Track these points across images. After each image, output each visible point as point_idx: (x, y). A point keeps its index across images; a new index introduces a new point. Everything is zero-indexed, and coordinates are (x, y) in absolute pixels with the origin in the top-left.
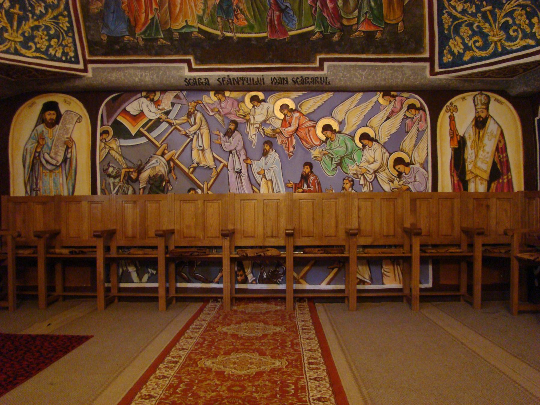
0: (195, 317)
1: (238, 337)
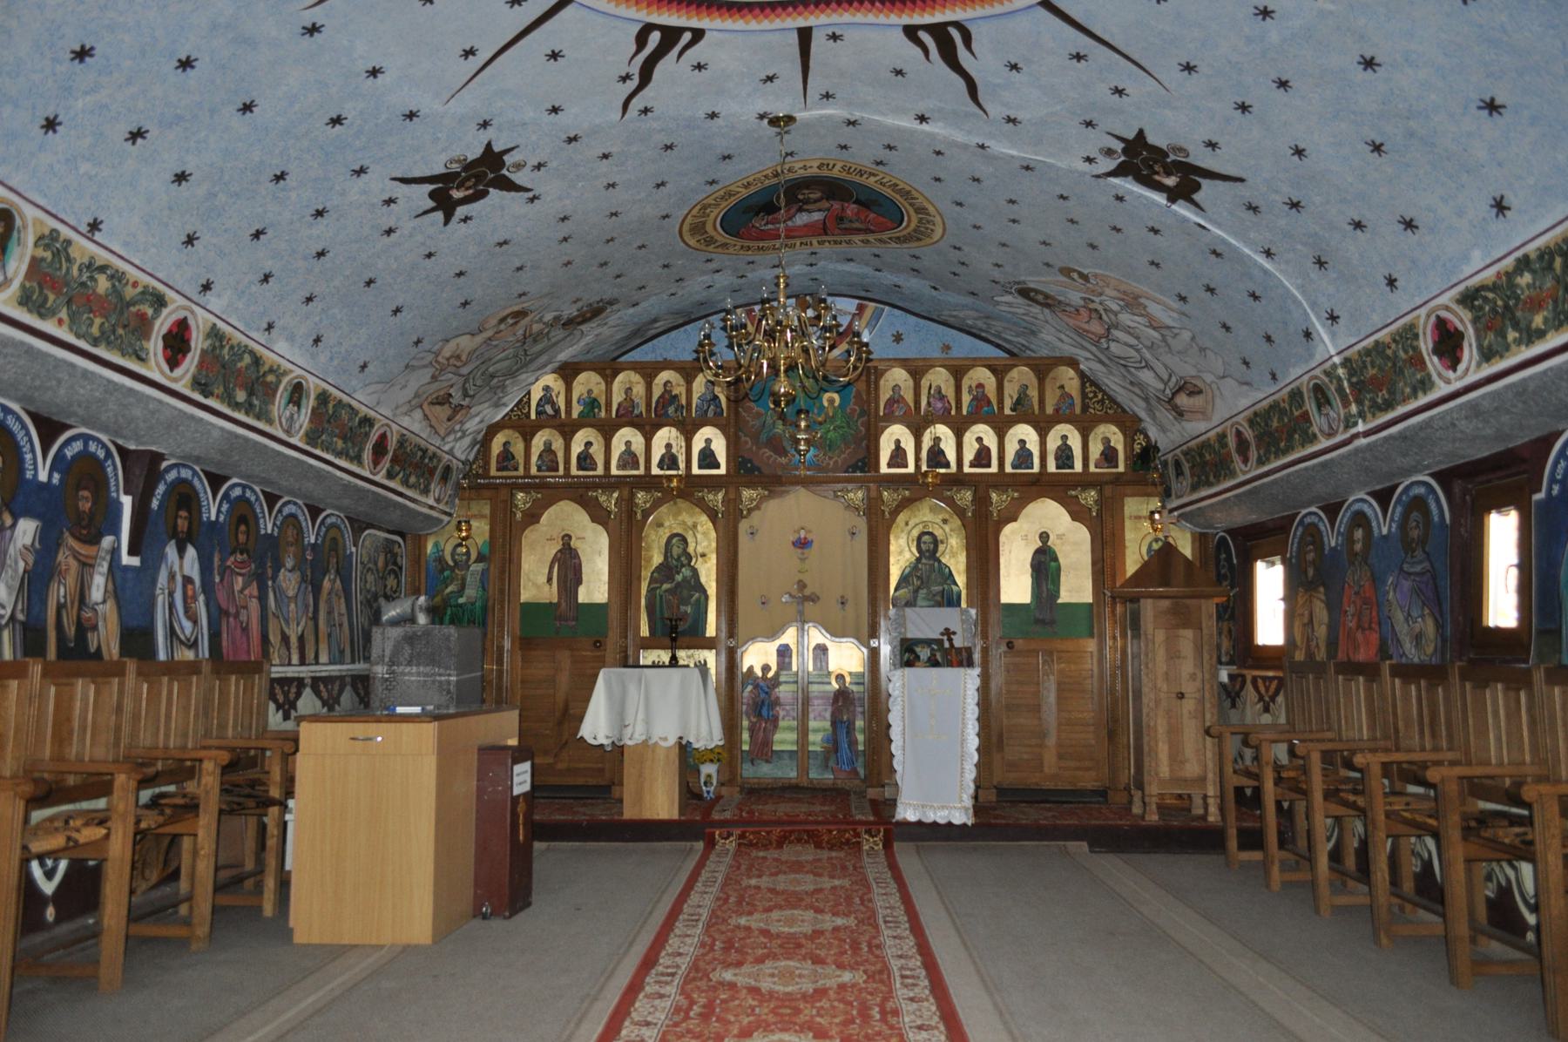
0: (701, 865)
1: (762, 995)
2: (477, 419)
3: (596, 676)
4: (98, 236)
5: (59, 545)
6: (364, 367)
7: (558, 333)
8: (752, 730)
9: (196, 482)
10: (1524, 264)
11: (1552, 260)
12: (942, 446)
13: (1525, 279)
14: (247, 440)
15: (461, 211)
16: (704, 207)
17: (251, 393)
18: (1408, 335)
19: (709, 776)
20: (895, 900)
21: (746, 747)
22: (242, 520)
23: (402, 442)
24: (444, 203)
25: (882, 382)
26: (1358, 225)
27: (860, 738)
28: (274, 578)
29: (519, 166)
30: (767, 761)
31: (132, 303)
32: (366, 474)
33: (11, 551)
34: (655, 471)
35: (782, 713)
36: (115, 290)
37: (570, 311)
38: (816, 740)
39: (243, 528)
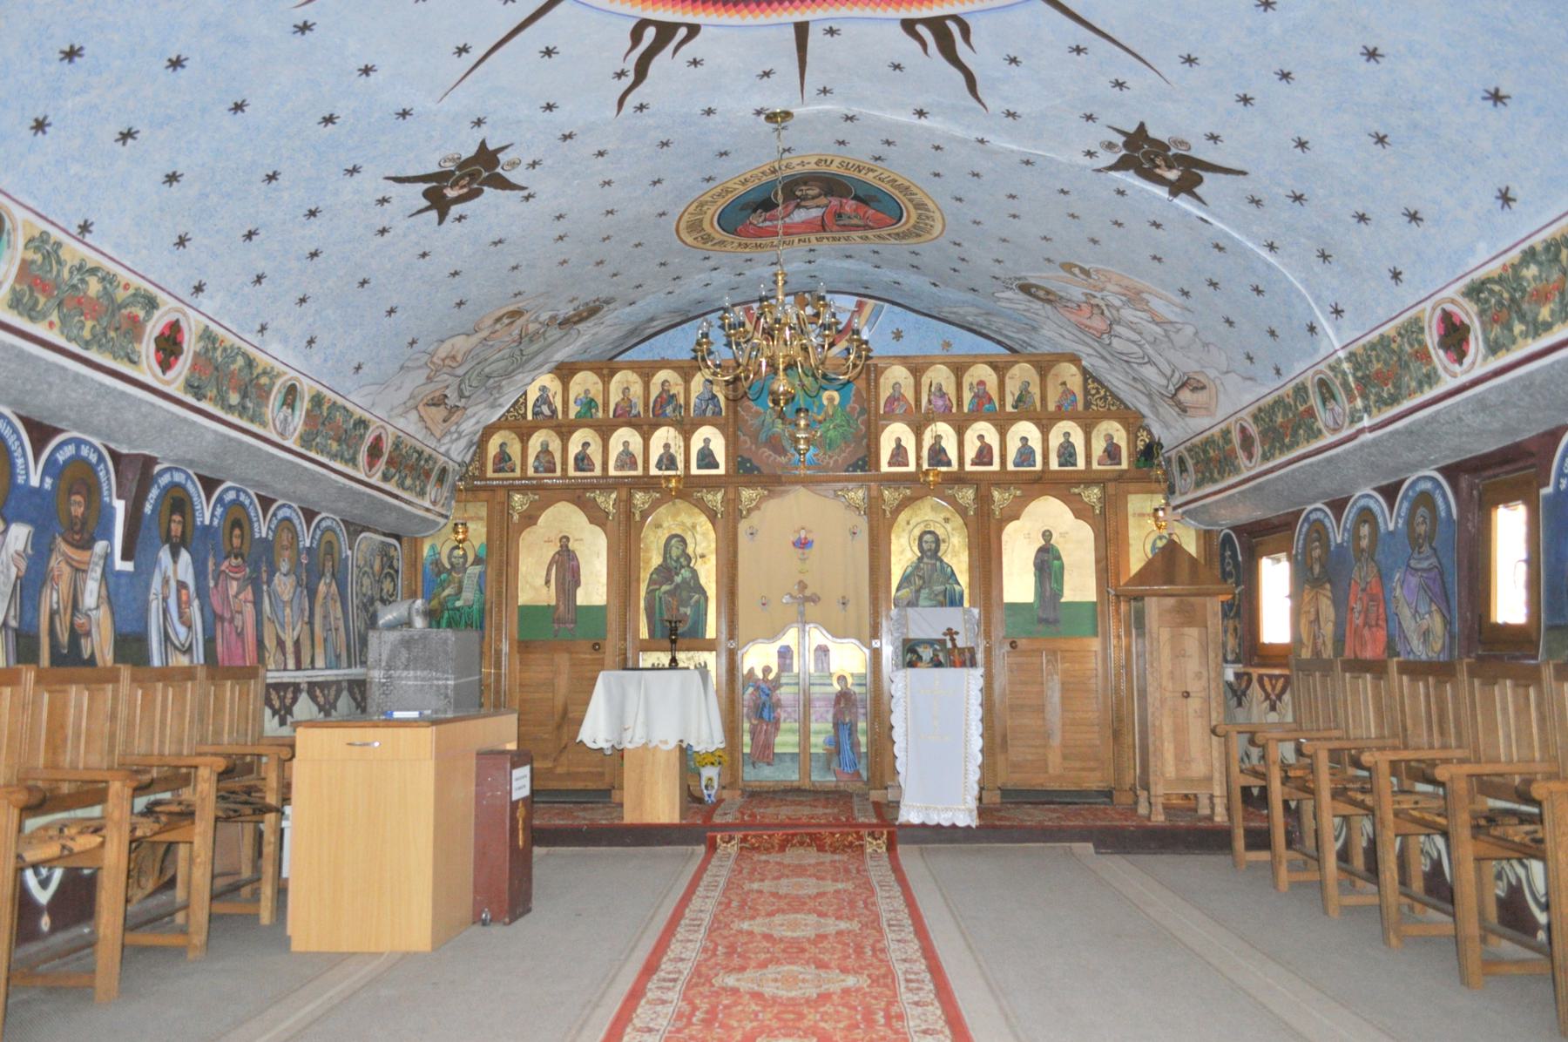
0: (702, 869)
2: (473, 420)
3: (595, 679)
4: (88, 238)
5: (51, 550)
6: (358, 368)
7: (555, 333)
8: (753, 733)
9: (190, 486)
10: (1530, 255)
12: (943, 444)
13: (1532, 271)
14: (240, 443)
15: (455, 210)
16: (701, 205)
17: (244, 396)
18: (1414, 328)
20: (899, 903)
21: (747, 750)
22: (237, 524)
25: (882, 380)
27: (863, 739)
28: (269, 583)
29: (514, 164)
30: (769, 764)
34: (654, 471)
35: (783, 715)
37: (567, 310)
38: (818, 743)
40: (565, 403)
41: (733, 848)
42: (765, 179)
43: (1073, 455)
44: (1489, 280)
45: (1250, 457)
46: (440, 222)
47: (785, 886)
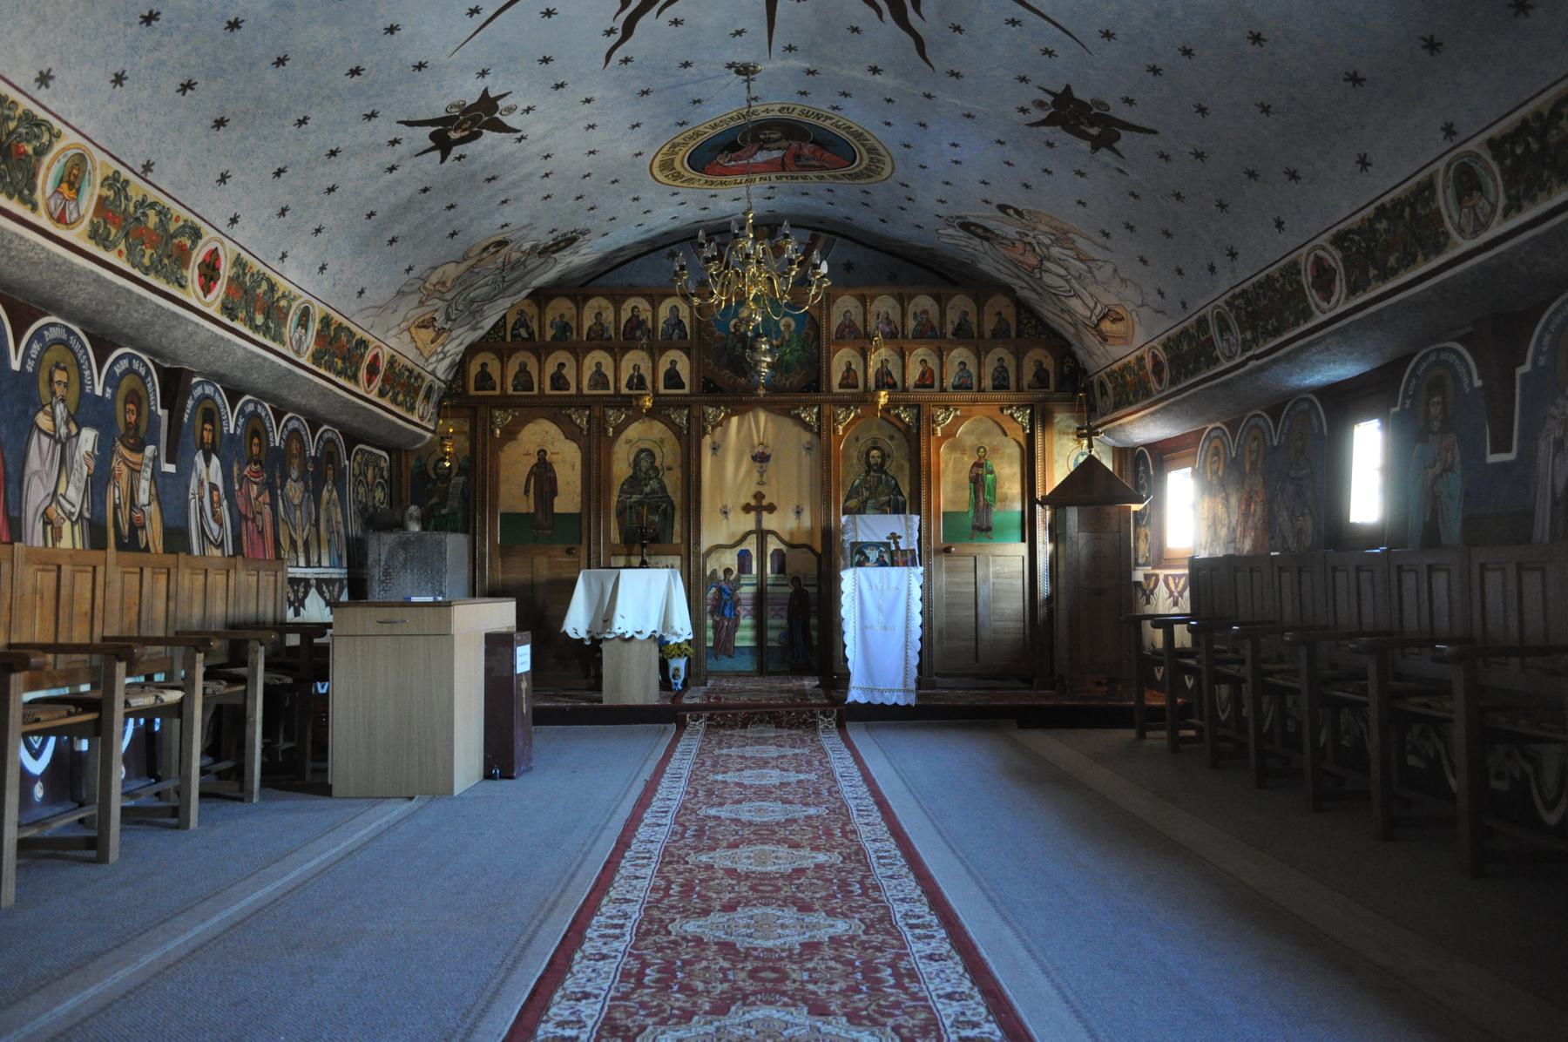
2: (457, 342)
3: (573, 583)
4: (150, 177)
5: (113, 453)
6: (361, 292)
7: (534, 262)
8: (716, 627)
9: (217, 398)
10: (1381, 212)
11: (1403, 211)
13: (1382, 225)
14: (265, 359)
15: (456, 151)
16: (674, 146)
17: (267, 318)
18: (1293, 270)
19: (677, 669)
20: (850, 762)
21: (710, 644)
22: (255, 433)
23: (392, 362)
24: (442, 144)
26: (1252, 174)
27: (814, 634)
28: (283, 487)
29: (510, 110)
31: (175, 236)
32: (361, 392)
33: (77, 457)
34: (624, 391)
36: (162, 224)
37: (548, 240)
39: (256, 441)
40: (541, 327)
41: (701, 726)
42: (732, 124)
43: (1007, 378)
44: (1350, 231)
45: (1160, 382)
46: (442, 161)
47: (749, 777)
